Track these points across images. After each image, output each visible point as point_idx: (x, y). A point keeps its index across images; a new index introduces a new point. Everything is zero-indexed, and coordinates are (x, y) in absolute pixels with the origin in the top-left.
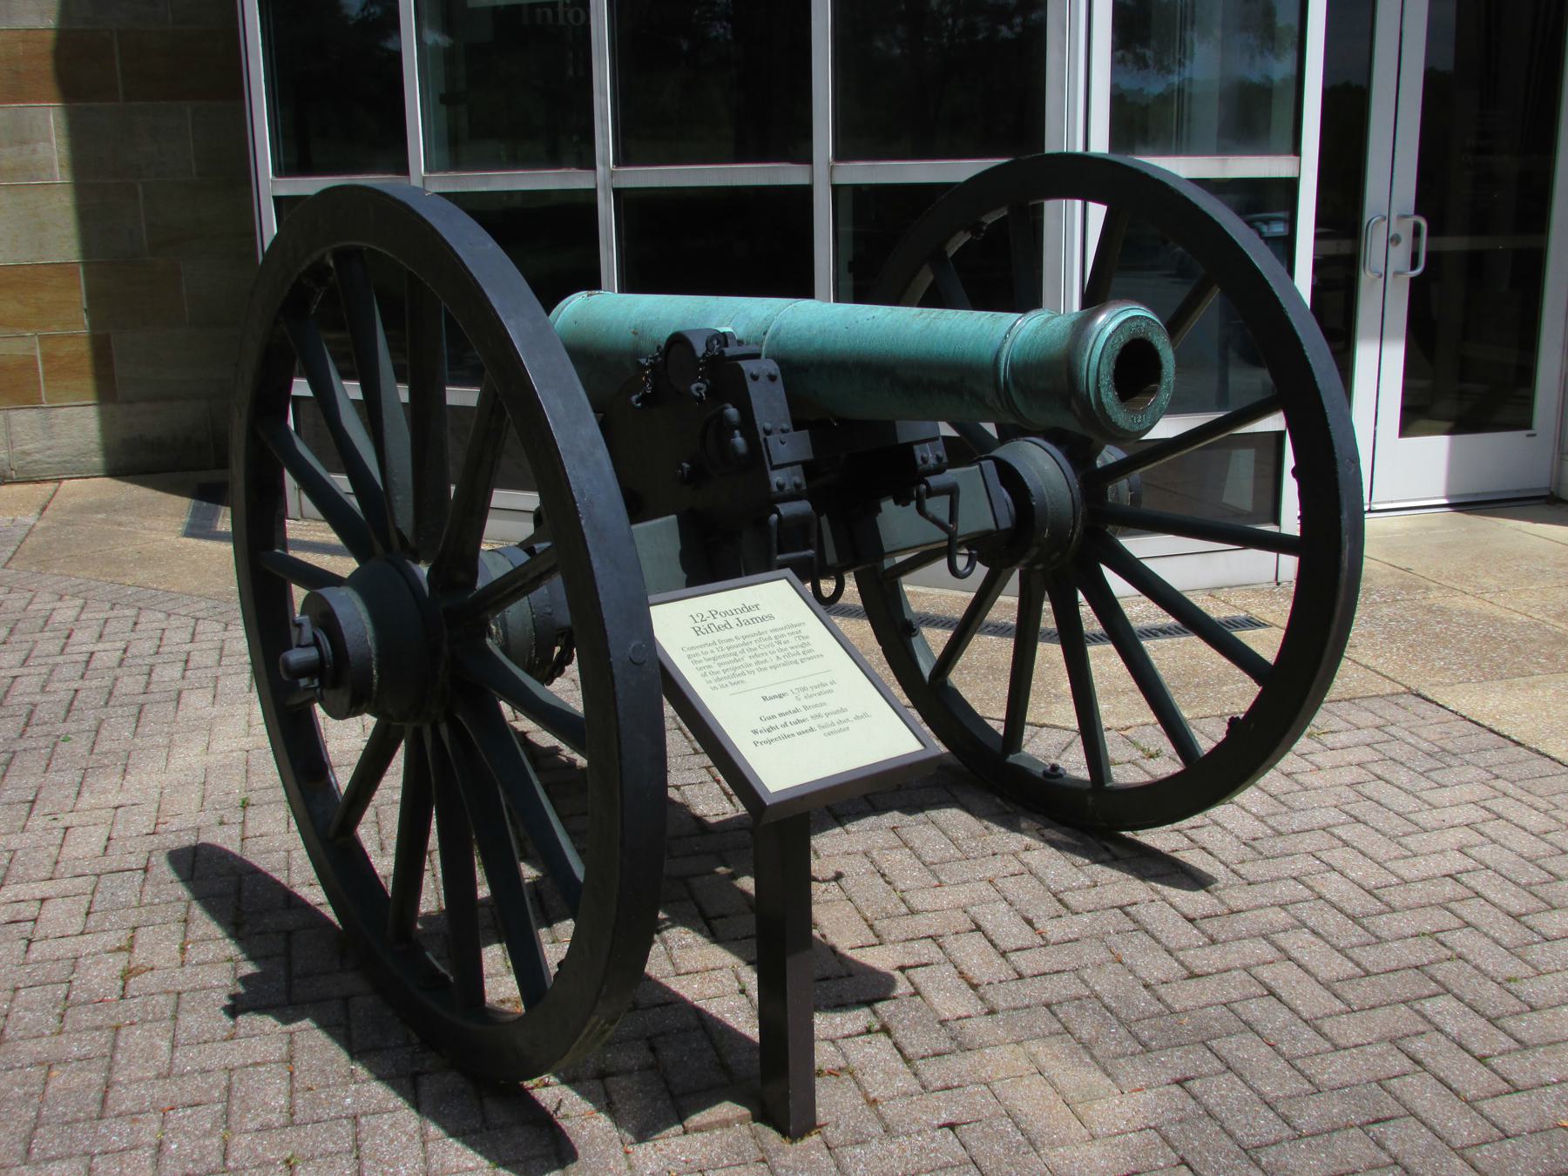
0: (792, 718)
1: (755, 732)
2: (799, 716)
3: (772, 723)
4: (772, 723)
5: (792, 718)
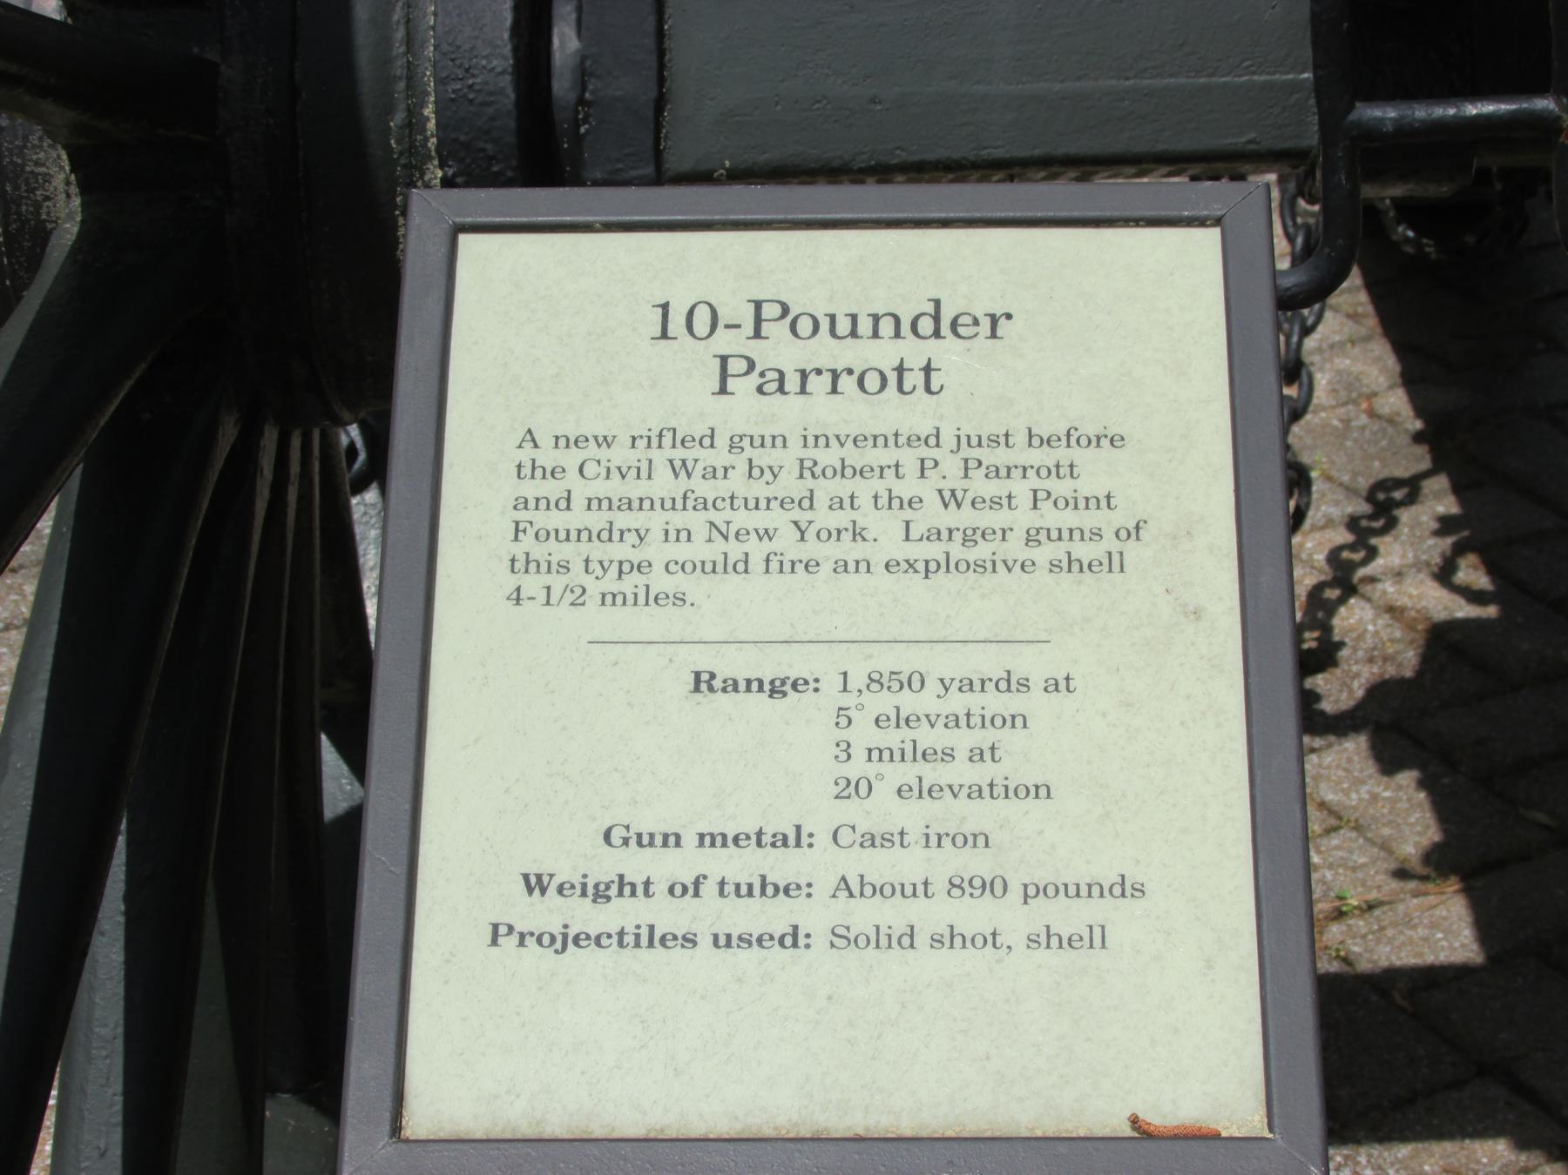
0: (740, 865)
1: (535, 884)
2: (781, 865)
3: (636, 864)
4: (636, 864)
5: (740, 865)
